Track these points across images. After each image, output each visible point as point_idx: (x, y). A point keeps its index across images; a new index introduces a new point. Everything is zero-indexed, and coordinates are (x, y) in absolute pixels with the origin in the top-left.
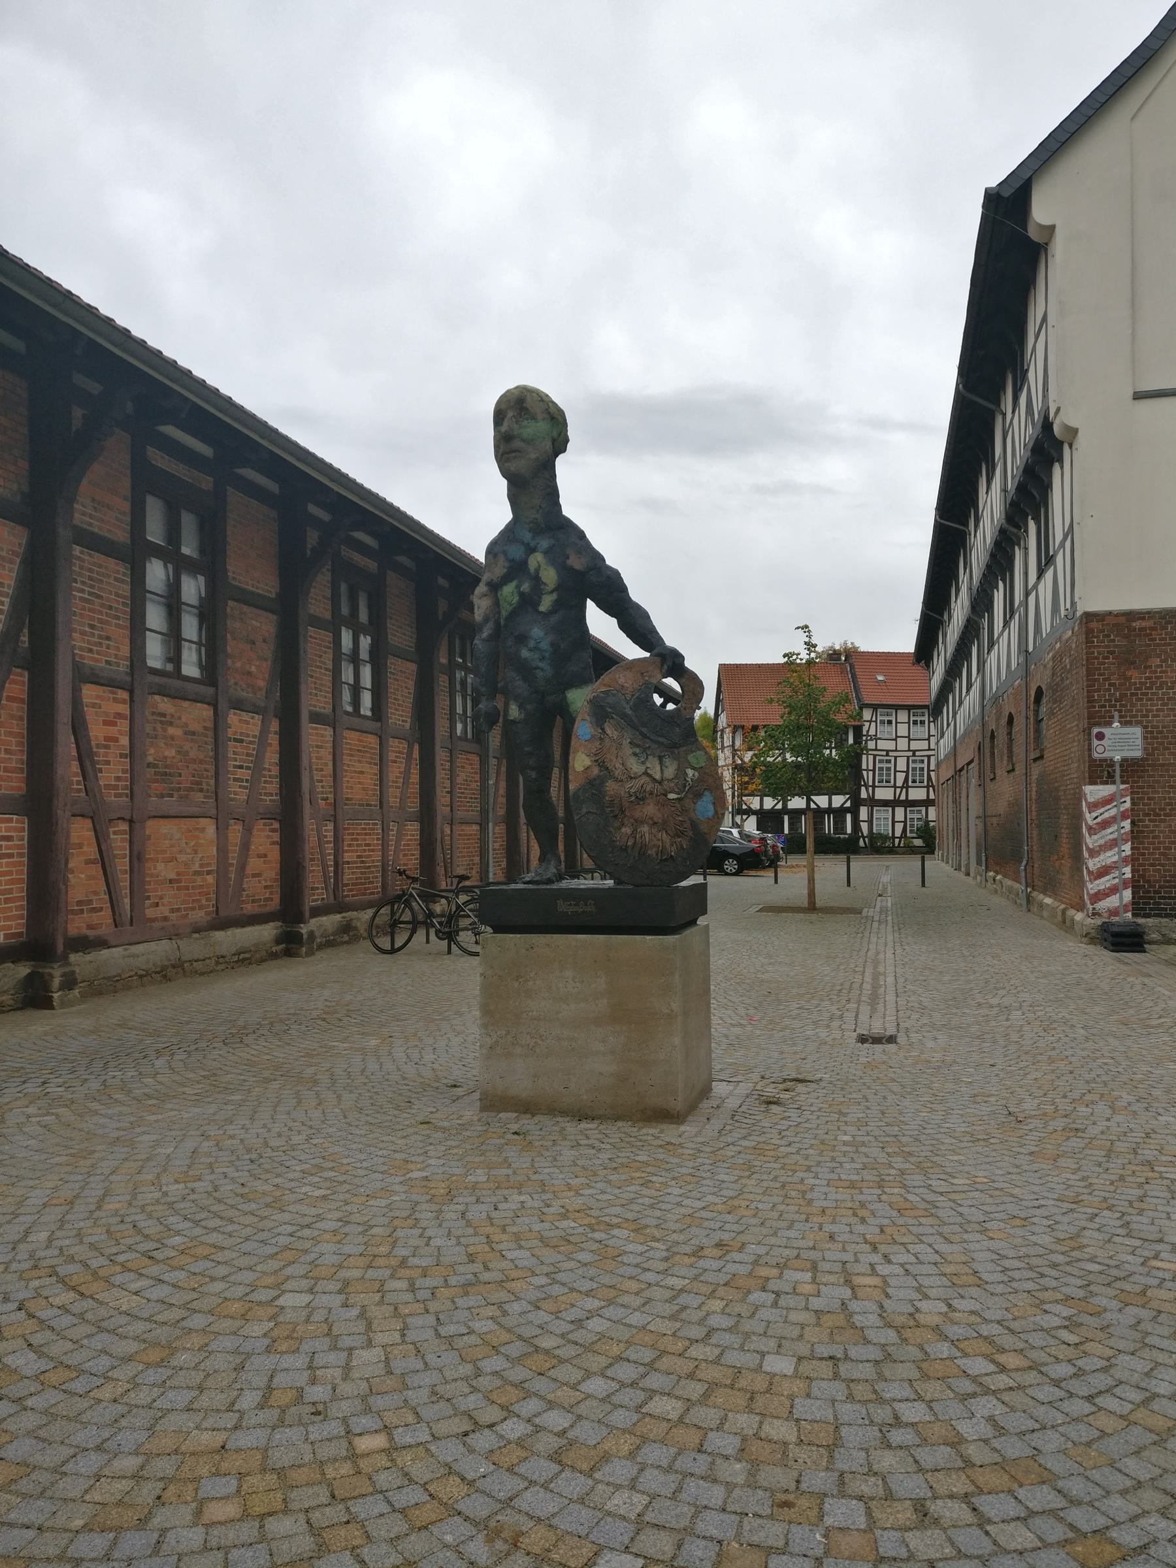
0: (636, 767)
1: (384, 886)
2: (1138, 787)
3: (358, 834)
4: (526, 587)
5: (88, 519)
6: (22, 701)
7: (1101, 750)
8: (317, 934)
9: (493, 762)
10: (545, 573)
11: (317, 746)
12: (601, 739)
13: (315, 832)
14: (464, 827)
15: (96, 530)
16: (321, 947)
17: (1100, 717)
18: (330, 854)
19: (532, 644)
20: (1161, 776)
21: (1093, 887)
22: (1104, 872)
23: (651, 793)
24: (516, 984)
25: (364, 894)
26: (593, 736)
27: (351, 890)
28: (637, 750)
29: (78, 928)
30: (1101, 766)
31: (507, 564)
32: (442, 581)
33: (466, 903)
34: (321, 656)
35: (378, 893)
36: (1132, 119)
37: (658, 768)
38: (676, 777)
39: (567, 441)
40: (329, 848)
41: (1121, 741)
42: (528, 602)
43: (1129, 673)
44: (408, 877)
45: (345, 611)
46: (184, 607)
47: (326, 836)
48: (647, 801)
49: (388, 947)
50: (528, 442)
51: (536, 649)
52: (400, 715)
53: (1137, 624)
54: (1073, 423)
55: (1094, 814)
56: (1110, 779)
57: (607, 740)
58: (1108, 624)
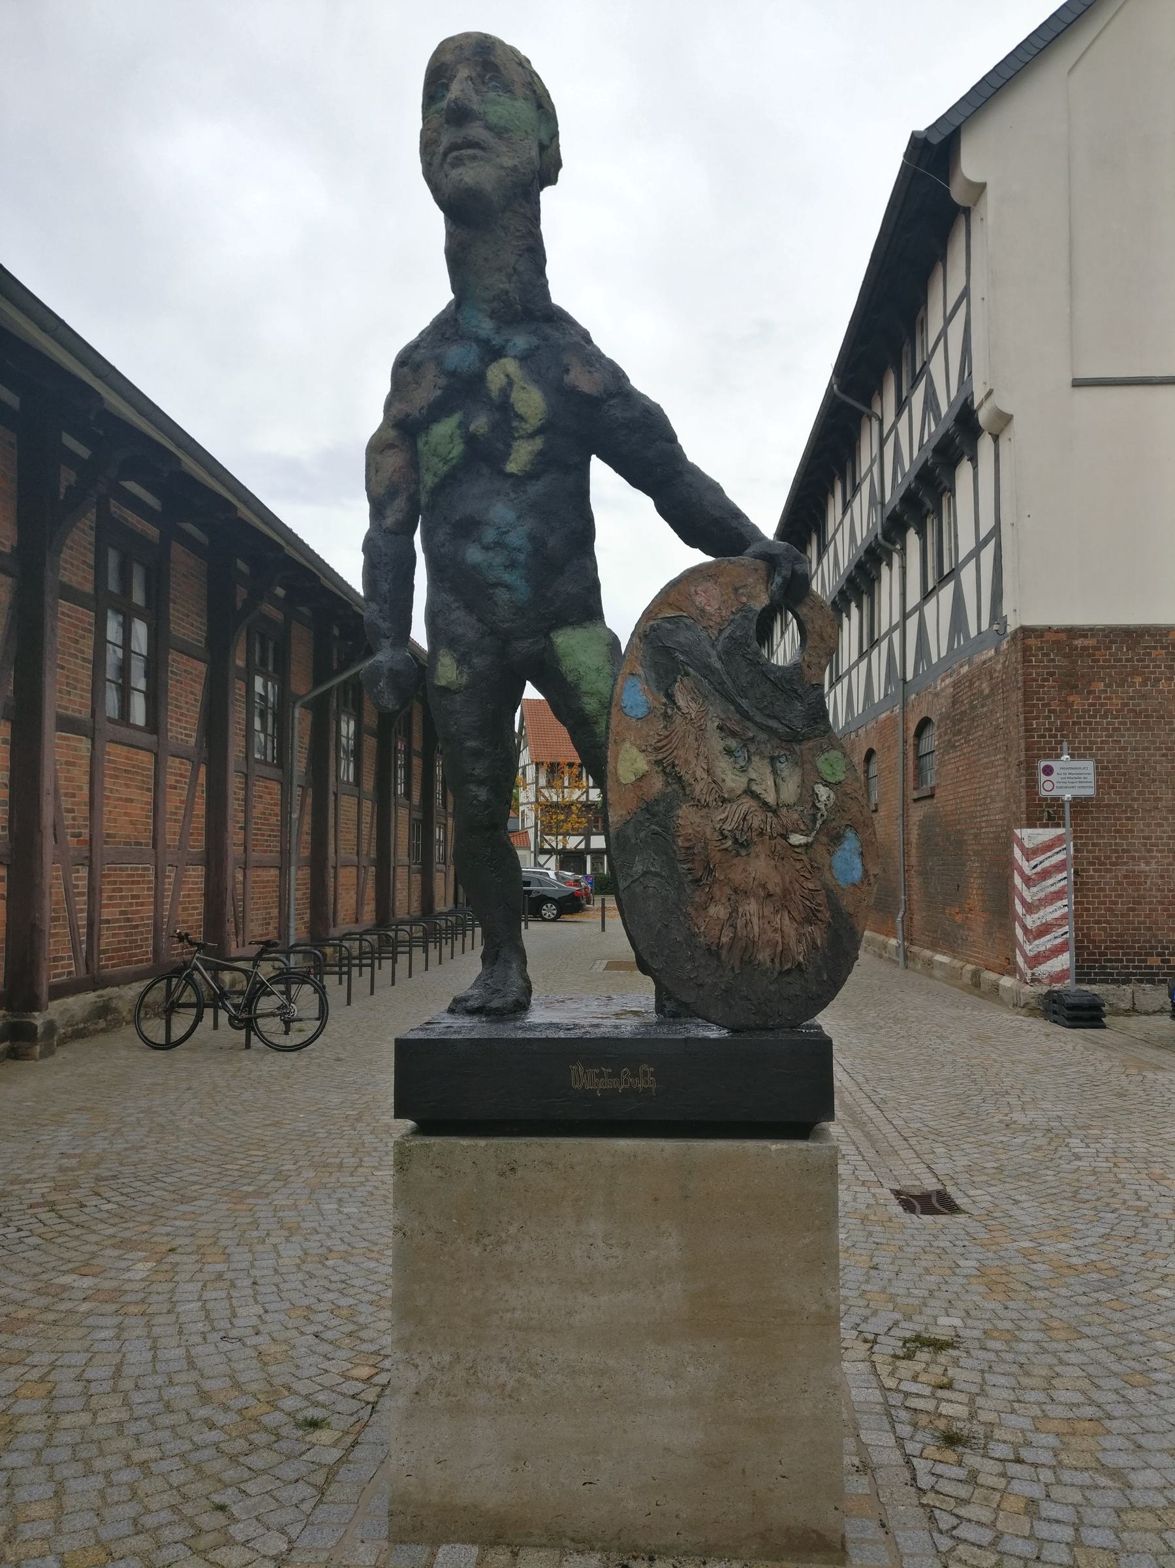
1: (156, 952)
2: (1082, 831)
3: (122, 883)
4: (480, 424)
7: (1048, 787)
8: (58, 1024)
9: (297, 791)
10: (524, 395)
11: (67, 763)
12: (666, 716)
13: (59, 880)
14: (260, 872)
16: (63, 1041)
17: (1039, 749)
18: (81, 911)
19: (490, 535)
20: (1107, 818)
21: (1031, 948)
22: (1044, 930)
24: (476, 1251)
25: (129, 963)
26: (651, 711)
27: (111, 958)
28: (733, 743)
30: (1041, 806)
31: (443, 381)
32: (242, 566)
34: (77, 642)
35: (148, 960)
36: (1070, 71)
37: (770, 782)
38: (800, 800)
39: (559, 165)
40: (81, 903)
41: (1070, 777)
42: (482, 455)
43: (1070, 699)
44: (192, 944)
45: (113, 586)
47: (77, 887)
48: (754, 849)
49: (160, 1039)
50: (500, 132)
51: (499, 545)
52: (184, 726)
53: (1079, 642)
54: (1007, 409)
55: (1033, 863)
56: (1054, 820)
57: (678, 719)
58: (1048, 641)
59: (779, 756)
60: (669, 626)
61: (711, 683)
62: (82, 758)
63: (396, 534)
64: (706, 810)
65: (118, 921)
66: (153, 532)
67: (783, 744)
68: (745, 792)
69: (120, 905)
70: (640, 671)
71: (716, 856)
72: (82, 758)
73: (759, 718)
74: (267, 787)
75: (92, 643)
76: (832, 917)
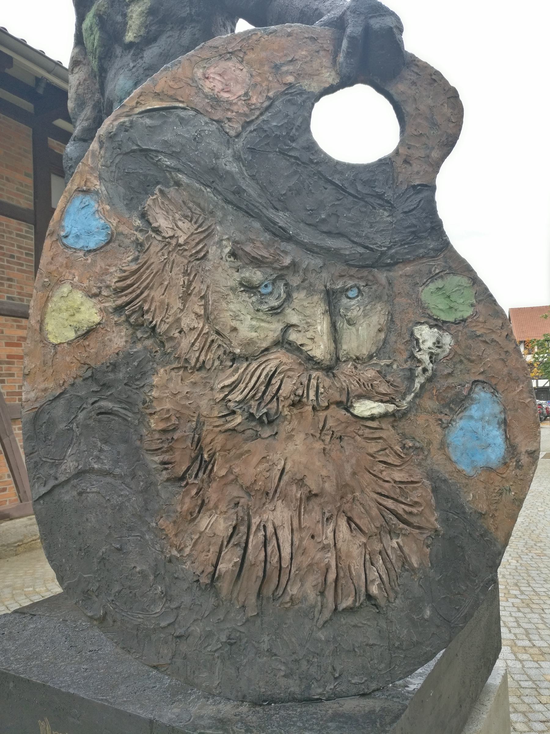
28: (256, 276)
48: (285, 428)
59: (344, 290)
60: (148, 121)
61: (216, 191)
64: (203, 374)
67: (353, 271)
70: (96, 184)
71: (214, 440)
73: (307, 236)
76: (445, 521)
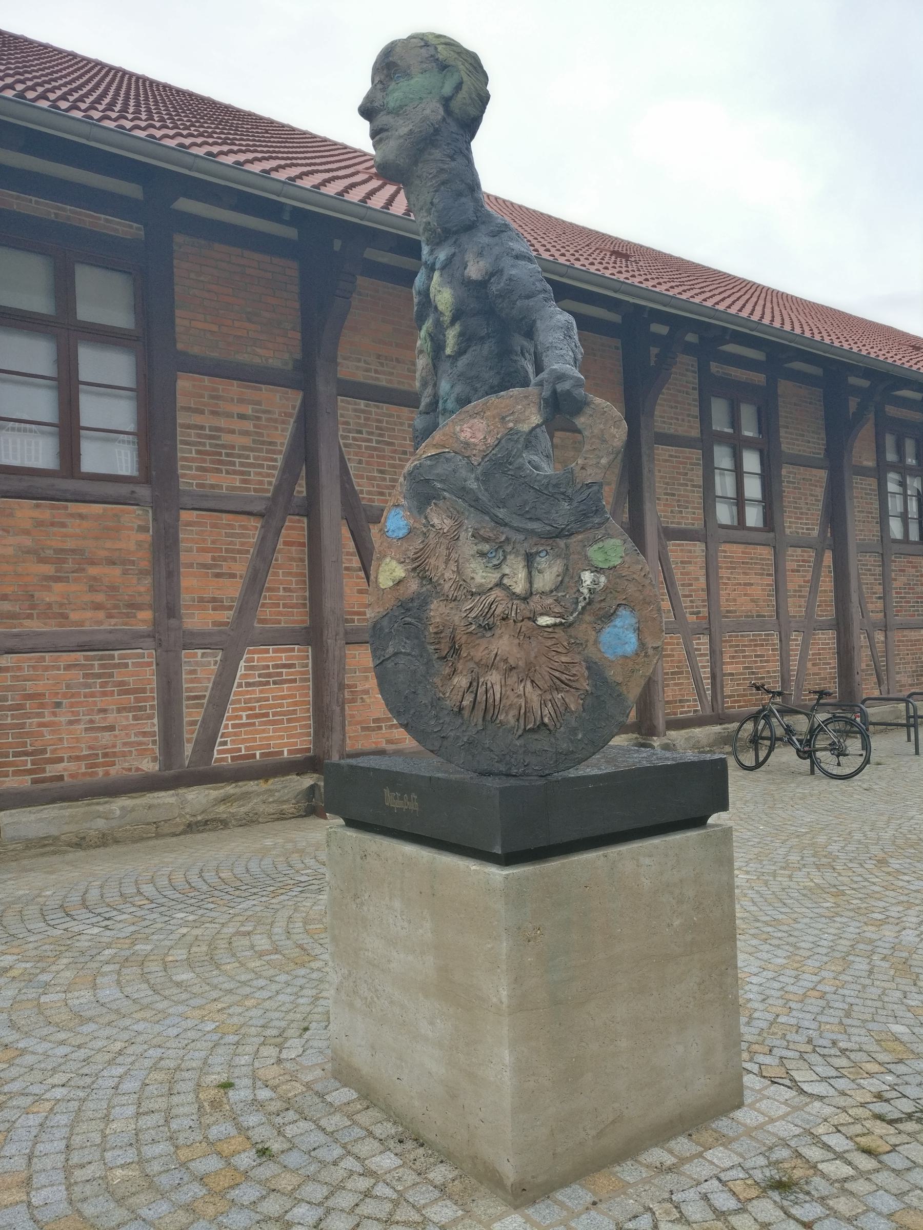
0: (480, 574)
5: (373, 374)
6: (303, 545)
15: (384, 383)
23: (505, 619)
28: (486, 547)
29: (374, 743)
33: (827, 722)
39: (484, 99)
44: (768, 692)
46: (83, 432)
48: (498, 632)
60: (429, 462)
62: (697, 557)
63: (427, 413)
64: (456, 603)
65: (742, 674)
66: (759, 378)
67: (543, 541)
68: (497, 585)
69: (744, 662)
70: (403, 502)
71: (462, 638)
72: (697, 557)
74: (911, 562)
75: (701, 473)
